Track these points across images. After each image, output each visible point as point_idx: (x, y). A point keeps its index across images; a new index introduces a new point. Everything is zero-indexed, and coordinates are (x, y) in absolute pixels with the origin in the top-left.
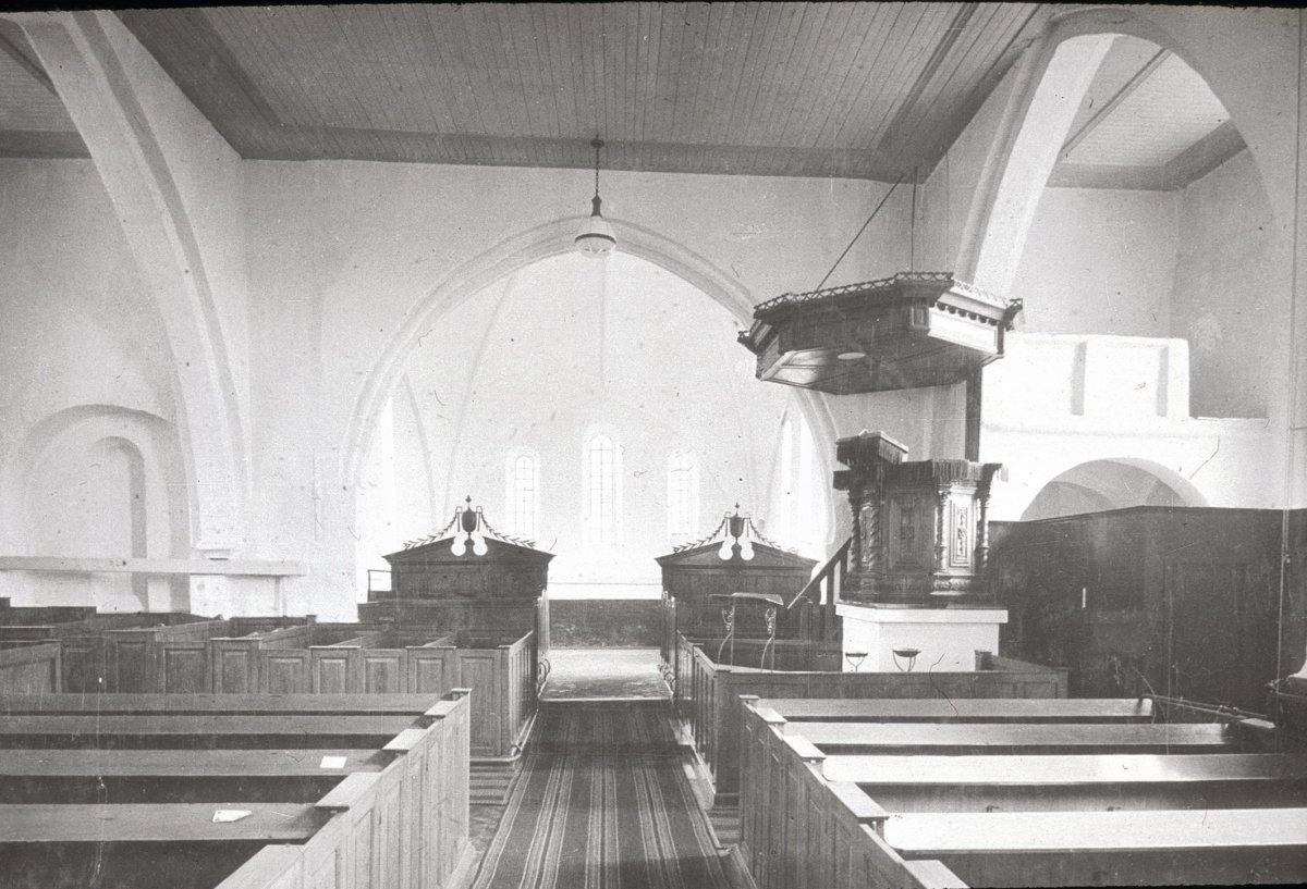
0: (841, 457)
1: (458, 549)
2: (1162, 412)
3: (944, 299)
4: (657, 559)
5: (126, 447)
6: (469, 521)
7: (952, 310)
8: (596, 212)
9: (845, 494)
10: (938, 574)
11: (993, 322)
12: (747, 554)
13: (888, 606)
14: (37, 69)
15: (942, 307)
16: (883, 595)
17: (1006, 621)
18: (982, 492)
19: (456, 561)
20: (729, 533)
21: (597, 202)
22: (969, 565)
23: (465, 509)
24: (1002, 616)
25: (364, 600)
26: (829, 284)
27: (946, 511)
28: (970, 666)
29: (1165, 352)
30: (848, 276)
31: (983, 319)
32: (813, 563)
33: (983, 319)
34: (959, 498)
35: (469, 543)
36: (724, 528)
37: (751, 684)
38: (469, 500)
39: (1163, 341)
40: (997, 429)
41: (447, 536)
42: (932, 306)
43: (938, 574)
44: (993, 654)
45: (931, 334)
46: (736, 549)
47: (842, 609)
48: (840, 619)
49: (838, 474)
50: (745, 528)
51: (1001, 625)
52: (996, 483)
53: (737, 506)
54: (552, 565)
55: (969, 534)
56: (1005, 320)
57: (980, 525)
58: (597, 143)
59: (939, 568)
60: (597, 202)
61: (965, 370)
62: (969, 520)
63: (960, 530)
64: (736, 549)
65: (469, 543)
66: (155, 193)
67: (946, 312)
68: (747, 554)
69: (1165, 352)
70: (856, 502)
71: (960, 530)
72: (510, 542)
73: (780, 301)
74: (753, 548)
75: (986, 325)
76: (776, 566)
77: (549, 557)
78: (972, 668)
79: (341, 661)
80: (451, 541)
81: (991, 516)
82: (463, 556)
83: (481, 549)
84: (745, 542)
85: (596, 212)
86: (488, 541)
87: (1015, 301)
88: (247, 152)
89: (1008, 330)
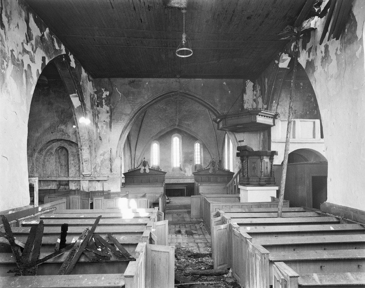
0: (238, 150)
1: (142, 171)
2: (314, 137)
5: (63, 148)
6: (145, 164)
7: (262, 116)
9: (239, 158)
11: (272, 118)
12: (148, 171)
18: (271, 159)
19: (142, 175)
27: (263, 163)
28: (270, 200)
29: (314, 123)
31: (269, 117)
32: (234, 173)
33: (269, 117)
34: (266, 160)
36: (141, 165)
37: (72, 254)
38: (144, 158)
39: (314, 120)
45: (258, 121)
48: (239, 189)
49: (237, 153)
51: (277, 190)
52: (275, 156)
55: (269, 168)
57: (271, 165)
65: (145, 170)
66: (258, 259)
67: (261, 116)
69: (314, 123)
70: (242, 160)
71: (266, 167)
75: (271, 118)
78: (270, 201)
80: (140, 169)
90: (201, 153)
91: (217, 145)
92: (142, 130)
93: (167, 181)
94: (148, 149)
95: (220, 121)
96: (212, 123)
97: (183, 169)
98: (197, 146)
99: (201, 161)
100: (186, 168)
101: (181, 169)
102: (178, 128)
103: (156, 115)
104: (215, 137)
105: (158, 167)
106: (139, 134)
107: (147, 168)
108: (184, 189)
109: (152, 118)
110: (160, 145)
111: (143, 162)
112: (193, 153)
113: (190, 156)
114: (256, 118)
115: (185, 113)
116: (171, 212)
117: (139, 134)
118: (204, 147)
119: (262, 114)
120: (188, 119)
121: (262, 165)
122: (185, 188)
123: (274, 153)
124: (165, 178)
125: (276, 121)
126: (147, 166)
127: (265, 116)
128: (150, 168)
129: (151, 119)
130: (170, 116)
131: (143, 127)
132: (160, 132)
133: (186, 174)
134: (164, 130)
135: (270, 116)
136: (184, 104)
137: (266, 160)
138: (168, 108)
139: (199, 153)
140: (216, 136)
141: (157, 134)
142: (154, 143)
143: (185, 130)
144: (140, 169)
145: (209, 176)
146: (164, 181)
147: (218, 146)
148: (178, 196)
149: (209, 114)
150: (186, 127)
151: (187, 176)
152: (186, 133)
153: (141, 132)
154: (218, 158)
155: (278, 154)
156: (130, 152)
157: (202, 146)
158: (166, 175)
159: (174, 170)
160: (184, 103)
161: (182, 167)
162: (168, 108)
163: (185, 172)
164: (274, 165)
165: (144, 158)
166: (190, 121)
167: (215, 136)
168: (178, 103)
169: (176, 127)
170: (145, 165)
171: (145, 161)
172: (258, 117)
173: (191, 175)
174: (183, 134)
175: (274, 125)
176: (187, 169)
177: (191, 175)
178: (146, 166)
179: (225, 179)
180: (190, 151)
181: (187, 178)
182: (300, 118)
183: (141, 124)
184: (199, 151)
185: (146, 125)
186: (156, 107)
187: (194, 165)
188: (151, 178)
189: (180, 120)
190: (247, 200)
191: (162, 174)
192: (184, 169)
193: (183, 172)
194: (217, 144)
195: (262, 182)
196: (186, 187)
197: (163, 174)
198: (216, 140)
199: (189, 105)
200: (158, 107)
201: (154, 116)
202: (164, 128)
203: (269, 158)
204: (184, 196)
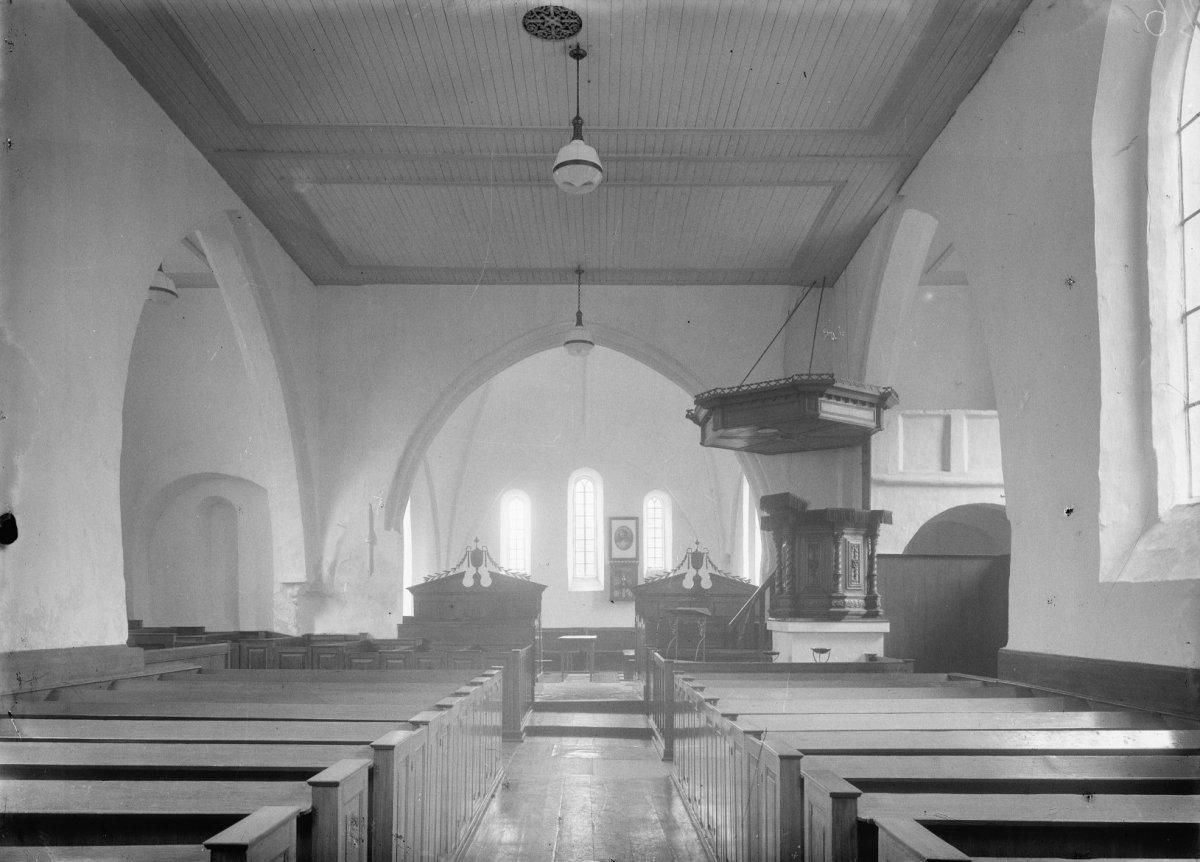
1: (468, 582)
3: (830, 391)
4: (546, 586)
6: (477, 558)
8: (579, 323)
10: (835, 595)
11: (872, 405)
12: (706, 584)
13: (798, 619)
14: (198, 250)
15: (830, 397)
16: (797, 614)
17: (888, 630)
18: (871, 535)
20: (691, 567)
21: (579, 315)
22: (862, 588)
23: (474, 548)
24: (885, 627)
25: (401, 622)
26: (747, 382)
30: (768, 372)
31: (864, 403)
34: (853, 539)
35: (477, 577)
36: (687, 561)
38: (477, 541)
40: (882, 483)
41: (458, 571)
42: (822, 397)
43: (835, 595)
44: (878, 655)
45: (823, 415)
46: (697, 579)
47: (773, 624)
48: (768, 635)
50: (704, 563)
51: (885, 634)
52: (883, 528)
53: (697, 543)
54: (545, 594)
56: (881, 402)
57: (871, 558)
58: (579, 271)
59: (836, 590)
60: (579, 315)
61: (858, 440)
62: (862, 554)
63: (853, 562)
64: (697, 579)
65: (477, 577)
68: (706, 584)
71: (853, 562)
72: (511, 575)
73: (712, 393)
74: (711, 579)
76: (729, 588)
77: (542, 588)
79: (400, 661)
80: (462, 575)
81: (879, 550)
82: (489, 588)
83: (486, 582)
84: (705, 573)
85: (579, 323)
86: (492, 575)
87: (886, 389)
88: (317, 281)
89: (885, 409)
95: (707, 419)
107: (484, 571)
114: (816, 408)
119: (839, 394)
121: (837, 553)
123: (882, 517)
125: (886, 415)
127: (855, 402)
135: (867, 399)
137: (853, 539)
144: (683, 576)
155: (894, 518)
164: (879, 556)
165: (697, 543)
172: (824, 402)
175: (879, 427)
182: (964, 408)
190: (236, 621)
195: (837, 607)
203: (863, 532)
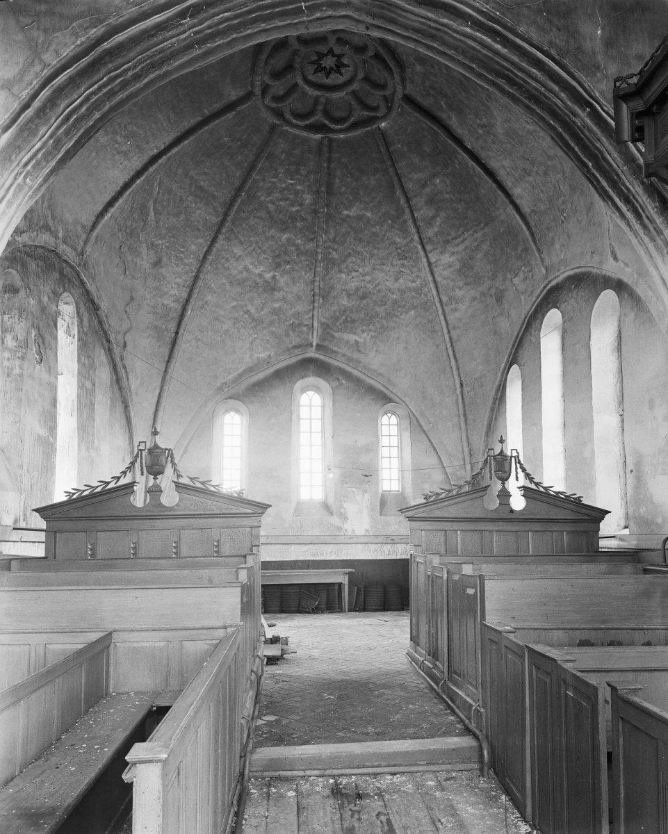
65: (154, 492)
80: (129, 487)
90: (401, 448)
91: (466, 419)
92: (178, 355)
93: (268, 554)
94: (203, 429)
96: (447, 337)
97: (334, 509)
98: (389, 426)
99: (402, 479)
100: (345, 505)
101: (326, 507)
102: (317, 356)
103: (234, 303)
104: (456, 389)
105: (241, 493)
106: (166, 371)
108: (340, 585)
109: (222, 313)
110: (251, 415)
111: (151, 451)
112: (372, 448)
113: (364, 459)
115: (344, 302)
116: (289, 764)
117: (166, 371)
118: (417, 427)
120: (356, 325)
122: (345, 580)
124: (262, 540)
126: (169, 470)
128: (181, 480)
129: (217, 319)
130: (291, 312)
131: (183, 346)
132: (250, 370)
133: (348, 526)
134: (268, 361)
136: (343, 266)
138: (282, 281)
139: (395, 452)
140: (462, 385)
141: (240, 375)
142: (227, 411)
143: (343, 366)
144: (129, 487)
145: (447, 526)
146: (254, 546)
147: (466, 423)
148: (316, 610)
149: (437, 299)
150: (348, 353)
151: (350, 533)
152: (348, 376)
153: (176, 366)
154: (468, 467)
156: (127, 436)
157: (406, 423)
158: (267, 519)
159: (299, 509)
160: (344, 261)
161: (331, 501)
162: (282, 281)
163: (344, 517)
166: (363, 331)
167: (458, 386)
168: (320, 257)
169: (312, 353)
170: (155, 470)
171: (156, 446)
173: (367, 530)
174: (338, 379)
176: (350, 508)
177: (367, 530)
178: (162, 473)
179: (562, 540)
180: (362, 441)
181: (352, 541)
183: (177, 333)
184: (395, 441)
185: (197, 340)
186: (234, 272)
187: (377, 492)
188: (186, 534)
189: (326, 327)
191: (246, 515)
192: (342, 506)
193: (335, 520)
194: (465, 415)
196: (350, 574)
197: (246, 515)
198: (460, 400)
199: (360, 270)
200: (245, 274)
201: (228, 307)
202: (263, 355)
204: (341, 612)
